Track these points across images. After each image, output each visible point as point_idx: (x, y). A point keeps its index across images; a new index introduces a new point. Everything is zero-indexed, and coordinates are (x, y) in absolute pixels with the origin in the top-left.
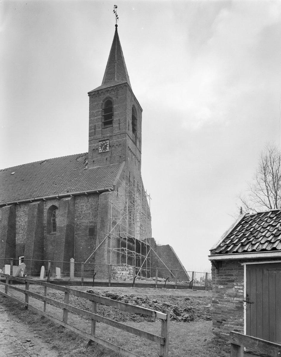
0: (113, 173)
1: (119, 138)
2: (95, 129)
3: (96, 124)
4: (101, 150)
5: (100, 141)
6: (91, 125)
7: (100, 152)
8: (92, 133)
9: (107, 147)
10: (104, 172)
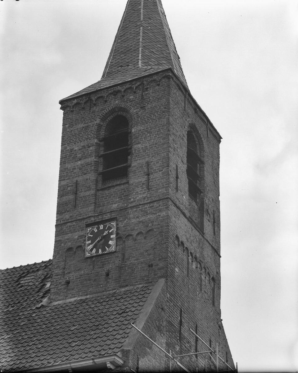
0: (125, 315)
1: (146, 213)
2: (76, 194)
3: (80, 179)
4: (92, 250)
5: (88, 226)
6: (64, 183)
7: (88, 255)
8: (66, 204)
9: (111, 239)
10: (99, 312)
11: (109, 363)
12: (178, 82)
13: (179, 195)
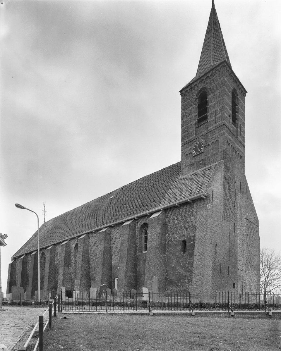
4: (195, 153)
7: (194, 155)
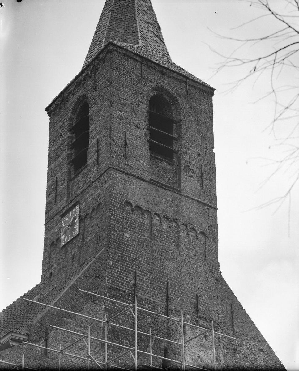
11: (10, 341)
12: (125, 52)
13: (131, 161)
